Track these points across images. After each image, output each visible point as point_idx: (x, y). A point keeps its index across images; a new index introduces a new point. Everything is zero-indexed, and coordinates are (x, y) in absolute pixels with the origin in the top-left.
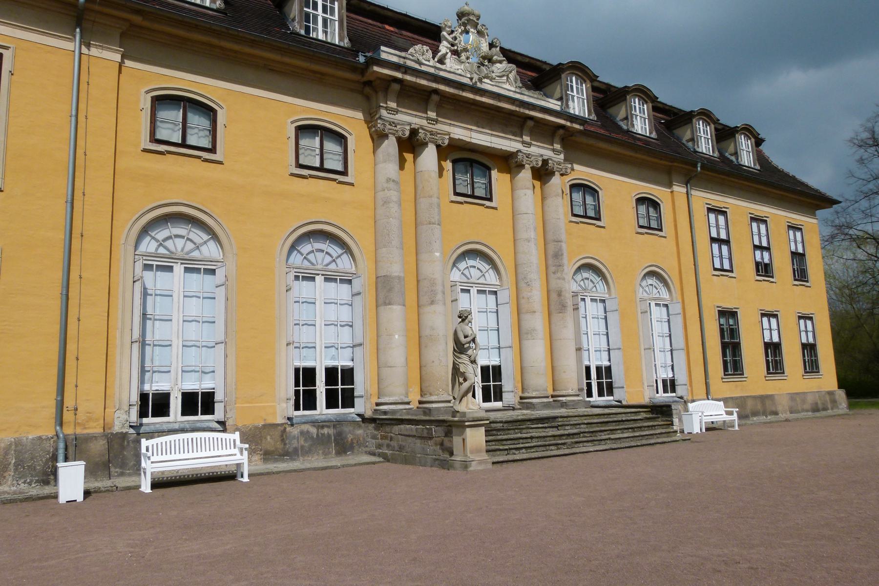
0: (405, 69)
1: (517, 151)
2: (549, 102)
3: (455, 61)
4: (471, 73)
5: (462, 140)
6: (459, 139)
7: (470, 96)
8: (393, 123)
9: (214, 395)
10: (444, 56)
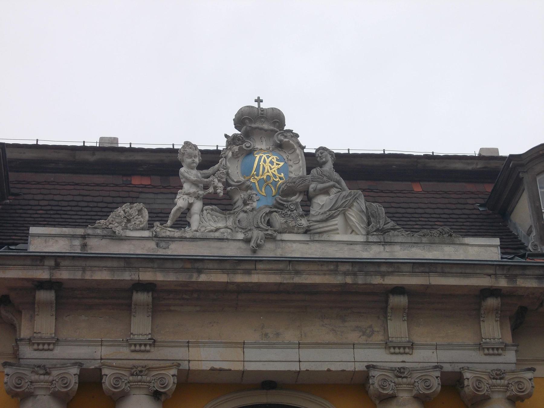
0: (56, 261)
1: (368, 367)
2: (468, 245)
3: (212, 215)
4: (245, 230)
5: (221, 370)
6: (213, 370)
7: (222, 278)
8: (44, 368)
9: (366, 366)
10: (188, 210)
